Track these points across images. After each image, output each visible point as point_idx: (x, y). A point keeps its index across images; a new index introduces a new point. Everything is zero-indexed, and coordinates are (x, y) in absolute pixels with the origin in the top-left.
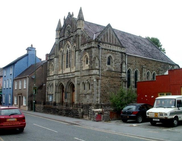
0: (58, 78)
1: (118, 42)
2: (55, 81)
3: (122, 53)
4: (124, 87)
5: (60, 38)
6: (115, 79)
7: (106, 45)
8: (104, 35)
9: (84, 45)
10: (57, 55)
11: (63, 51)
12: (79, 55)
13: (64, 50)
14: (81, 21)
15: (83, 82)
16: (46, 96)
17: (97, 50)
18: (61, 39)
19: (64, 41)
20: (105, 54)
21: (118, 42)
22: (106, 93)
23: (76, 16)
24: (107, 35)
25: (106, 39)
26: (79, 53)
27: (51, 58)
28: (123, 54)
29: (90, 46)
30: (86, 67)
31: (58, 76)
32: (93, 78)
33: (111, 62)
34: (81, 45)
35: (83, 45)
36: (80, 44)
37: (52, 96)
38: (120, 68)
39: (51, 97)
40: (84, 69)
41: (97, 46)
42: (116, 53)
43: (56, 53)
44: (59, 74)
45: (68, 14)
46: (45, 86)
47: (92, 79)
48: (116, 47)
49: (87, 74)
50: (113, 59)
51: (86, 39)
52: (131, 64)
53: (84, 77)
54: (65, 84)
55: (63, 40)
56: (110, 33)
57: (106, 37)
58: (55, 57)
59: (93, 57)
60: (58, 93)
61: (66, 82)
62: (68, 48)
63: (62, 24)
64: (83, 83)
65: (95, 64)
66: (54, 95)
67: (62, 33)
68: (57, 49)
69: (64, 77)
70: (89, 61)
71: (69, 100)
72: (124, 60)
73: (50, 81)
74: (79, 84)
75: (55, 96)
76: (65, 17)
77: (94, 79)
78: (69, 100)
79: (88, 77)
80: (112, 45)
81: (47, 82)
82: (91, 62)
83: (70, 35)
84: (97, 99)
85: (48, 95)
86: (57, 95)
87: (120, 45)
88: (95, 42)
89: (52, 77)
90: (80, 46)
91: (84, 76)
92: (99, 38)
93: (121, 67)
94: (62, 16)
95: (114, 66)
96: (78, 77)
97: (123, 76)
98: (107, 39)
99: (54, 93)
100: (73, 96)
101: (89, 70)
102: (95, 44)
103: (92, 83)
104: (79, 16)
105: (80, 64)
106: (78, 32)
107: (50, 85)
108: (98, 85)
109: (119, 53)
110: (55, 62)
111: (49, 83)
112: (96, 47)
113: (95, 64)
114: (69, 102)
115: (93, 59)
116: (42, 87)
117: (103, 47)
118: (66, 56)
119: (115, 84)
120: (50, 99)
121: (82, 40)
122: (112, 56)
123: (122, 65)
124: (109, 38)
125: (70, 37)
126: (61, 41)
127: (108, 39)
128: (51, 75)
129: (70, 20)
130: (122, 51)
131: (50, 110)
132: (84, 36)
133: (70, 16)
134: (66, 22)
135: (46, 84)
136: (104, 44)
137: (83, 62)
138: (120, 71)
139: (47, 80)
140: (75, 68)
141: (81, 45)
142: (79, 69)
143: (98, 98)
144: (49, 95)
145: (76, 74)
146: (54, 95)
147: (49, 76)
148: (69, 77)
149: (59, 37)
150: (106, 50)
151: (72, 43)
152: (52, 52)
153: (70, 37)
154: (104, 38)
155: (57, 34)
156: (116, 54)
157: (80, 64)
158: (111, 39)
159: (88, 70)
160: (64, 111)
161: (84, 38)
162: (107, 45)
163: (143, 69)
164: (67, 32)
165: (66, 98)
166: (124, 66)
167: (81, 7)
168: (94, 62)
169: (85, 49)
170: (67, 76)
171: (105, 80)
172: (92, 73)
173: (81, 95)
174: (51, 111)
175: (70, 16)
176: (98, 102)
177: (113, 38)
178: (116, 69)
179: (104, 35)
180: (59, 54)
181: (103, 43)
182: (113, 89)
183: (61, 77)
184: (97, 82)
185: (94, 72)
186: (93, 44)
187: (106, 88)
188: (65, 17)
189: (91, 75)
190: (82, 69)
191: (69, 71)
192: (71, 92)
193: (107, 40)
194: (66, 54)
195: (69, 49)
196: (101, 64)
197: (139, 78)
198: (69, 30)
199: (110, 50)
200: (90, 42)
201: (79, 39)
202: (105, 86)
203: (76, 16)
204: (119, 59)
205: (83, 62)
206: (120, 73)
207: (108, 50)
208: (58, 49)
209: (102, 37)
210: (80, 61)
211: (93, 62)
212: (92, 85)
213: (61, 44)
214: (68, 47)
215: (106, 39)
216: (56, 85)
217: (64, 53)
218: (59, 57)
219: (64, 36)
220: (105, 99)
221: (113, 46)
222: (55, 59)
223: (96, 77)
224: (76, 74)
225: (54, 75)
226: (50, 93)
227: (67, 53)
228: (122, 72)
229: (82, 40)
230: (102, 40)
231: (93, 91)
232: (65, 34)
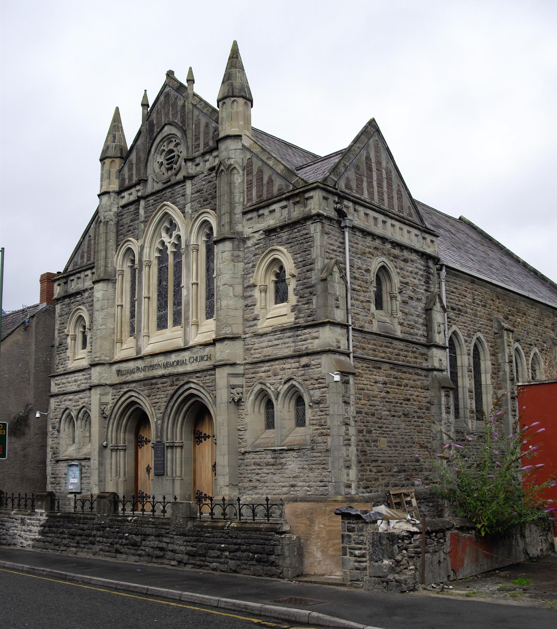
0: (116, 380)
2: (101, 395)
3: (424, 255)
4: (444, 415)
5: (119, 193)
6: (408, 378)
7: (366, 215)
8: (357, 167)
9: (261, 212)
10: (110, 269)
11: (142, 247)
12: (235, 259)
13: (147, 246)
14: (241, 101)
15: (262, 390)
16: (49, 470)
17: (334, 231)
18: (126, 194)
19: (142, 203)
20: (364, 253)
22: (376, 441)
23: (209, 90)
24: (370, 169)
25: (365, 184)
26: (236, 253)
27: (73, 287)
28: (431, 264)
29: (297, 213)
31: (115, 368)
32: (324, 370)
33: (386, 298)
34: (244, 213)
36: (239, 209)
37: (81, 467)
38: (423, 324)
39: (76, 471)
40: (263, 325)
41: (333, 214)
42: (406, 254)
43: (102, 263)
44: (117, 357)
46: (44, 418)
47: (314, 372)
48: (406, 228)
50: (396, 280)
51: (270, 181)
52: (459, 310)
53: (266, 367)
55: (139, 199)
56: (379, 163)
57: (365, 179)
58: (94, 283)
59: (318, 265)
60: (115, 449)
61: (162, 398)
62: (164, 234)
63: (132, 127)
64: (263, 395)
65: (331, 301)
66: (94, 462)
67: (130, 169)
68: (107, 241)
70: (292, 285)
71: (178, 484)
72: (434, 289)
73: (71, 397)
74: (238, 403)
75: (101, 464)
76: (145, 97)
77: (328, 369)
78: (178, 484)
79: (291, 364)
81: (53, 401)
82: (307, 291)
83: (176, 175)
85: (57, 461)
86: (108, 461)
88: (325, 194)
90: (238, 216)
91: (268, 361)
92: (340, 176)
93: (428, 324)
94: (129, 104)
95: (400, 314)
96: (234, 365)
97: (437, 365)
98: (370, 184)
99: (92, 448)
100: (195, 460)
101: (296, 328)
102: (324, 203)
103: (317, 394)
104: (228, 78)
105: (241, 303)
106: (223, 155)
107: (69, 414)
108: (346, 403)
109: (414, 257)
110: (97, 306)
111: (63, 407)
113: (329, 297)
114: (178, 492)
115: (314, 277)
116: (27, 425)
118: (155, 269)
119: (409, 400)
120: (73, 480)
121: (249, 189)
122: (390, 266)
123: (428, 311)
124: (375, 184)
125: (178, 183)
126: (123, 207)
127: (373, 188)
128: (72, 365)
129: (174, 105)
130: (428, 251)
132: (260, 171)
133: (176, 91)
134: (154, 115)
135: (45, 408)
137: (256, 293)
138: (423, 340)
139: (54, 389)
142: (238, 329)
143: (348, 467)
144: (63, 465)
145: (222, 352)
146: (94, 462)
147: (61, 370)
149: (115, 187)
150: (369, 239)
152: (78, 259)
153: (178, 183)
154: (360, 181)
155: (105, 177)
156: (405, 261)
157: (241, 303)
158: (385, 189)
159: (291, 329)
160: (179, 540)
161: (260, 179)
162: (372, 213)
163: (501, 337)
164: (157, 160)
165: (160, 471)
166: (438, 317)
168: (326, 290)
169: (269, 232)
170: (166, 366)
171: (373, 380)
172: (315, 345)
173: (252, 455)
174: (93, 543)
175: (176, 91)
176: (349, 486)
177: (390, 185)
178: (408, 329)
179: (357, 167)
180: (119, 262)
181: (355, 203)
182: (403, 425)
183: (132, 372)
184: (341, 387)
185: (327, 336)
186: (316, 203)
187: (375, 419)
188: (145, 97)
189: (308, 354)
191: (132, 353)
192: (188, 443)
193: (371, 194)
194: (155, 262)
195: (173, 240)
196: (353, 301)
197: (489, 376)
198: (171, 151)
199: (384, 240)
200: (298, 194)
201: (230, 184)
202: (373, 409)
203: (209, 90)
204: (416, 281)
205: (256, 293)
208: (112, 242)
209: (351, 174)
210: (239, 289)
211: (319, 288)
212: (318, 403)
213: (126, 220)
214: (168, 231)
215: (365, 184)
217: (145, 258)
218: (119, 278)
219: (143, 181)
222: (99, 287)
223: (339, 362)
224: (222, 352)
225: (93, 365)
226: (70, 451)
228: (430, 345)
229: (249, 189)
230: (351, 189)
231: (322, 434)
232: (149, 171)
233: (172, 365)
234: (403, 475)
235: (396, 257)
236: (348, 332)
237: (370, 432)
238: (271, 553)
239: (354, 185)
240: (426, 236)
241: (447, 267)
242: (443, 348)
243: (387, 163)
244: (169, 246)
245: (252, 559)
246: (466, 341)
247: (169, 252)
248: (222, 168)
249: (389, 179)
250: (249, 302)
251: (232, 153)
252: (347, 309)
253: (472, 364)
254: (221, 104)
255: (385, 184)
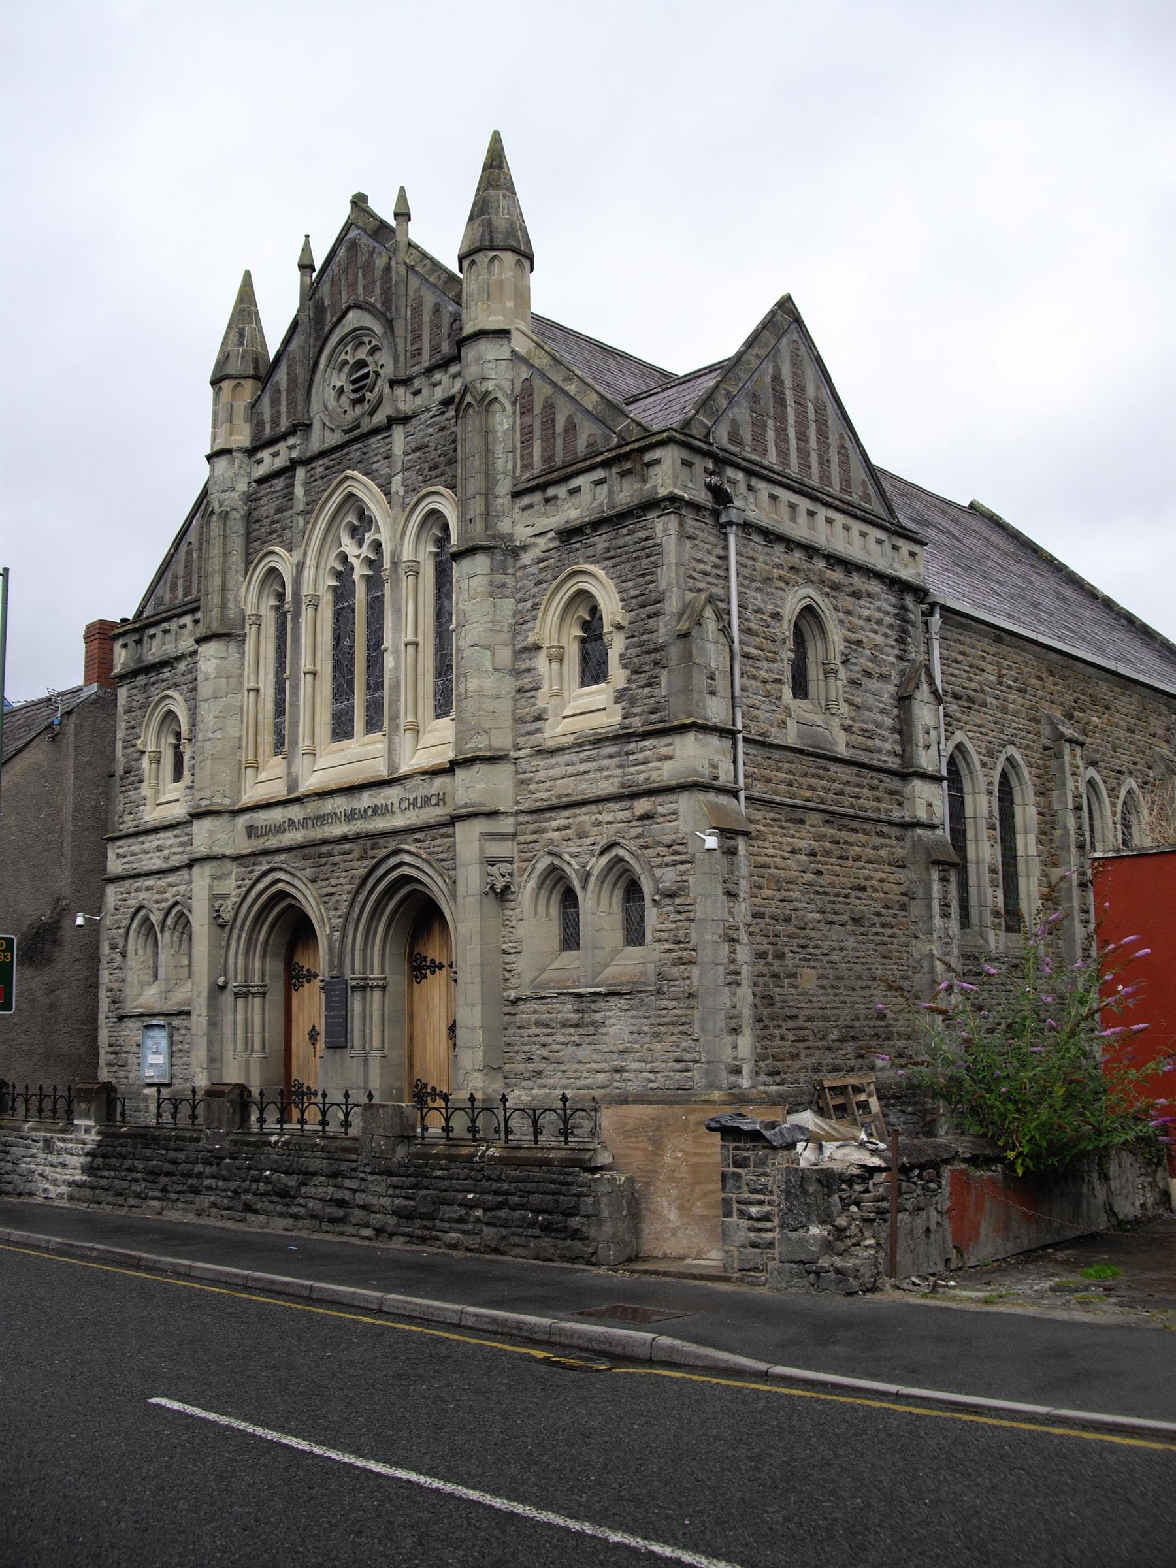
0: (245, 846)
1: (864, 483)
4: (938, 921)
5: (251, 452)
6: (861, 842)
8: (755, 398)
9: (551, 492)
10: (232, 613)
11: (300, 567)
12: (496, 591)
13: (310, 565)
14: (509, 258)
15: (553, 869)
16: (103, 1036)
17: (705, 532)
18: (265, 454)
19: (300, 473)
21: (864, 482)
22: (794, 975)
23: (440, 234)
24: (780, 401)
25: (771, 434)
26: (499, 579)
27: (155, 650)
28: (909, 601)
29: (626, 493)
30: (586, 706)
31: (243, 820)
32: (683, 826)
33: (814, 673)
34: (516, 495)
35: (539, 486)
36: (504, 487)
37: (172, 1031)
38: (893, 729)
39: (160, 1038)
40: (555, 731)
41: (703, 497)
42: (857, 580)
43: (215, 599)
45: (343, 212)
46: (93, 928)
47: (663, 830)
49: (608, 787)
50: (837, 636)
51: (571, 427)
52: (970, 699)
53: (561, 819)
54: (325, 898)
55: (288, 471)
56: (800, 389)
57: (770, 422)
59: (672, 604)
60: (244, 993)
61: (342, 884)
62: (346, 539)
63: (278, 313)
64: (555, 878)
65: (700, 681)
67: (275, 402)
68: (225, 554)
69: (318, 833)
70: (616, 646)
71: (375, 1065)
72: (916, 654)
73: (150, 882)
74: (502, 895)
75: (214, 1023)
76: (307, 249)
77: (693, 824)
78: (375, 1065)
79: (615, 813)
80: (827, 505)
81: (111, 891)
82: (648, 659)
83: (372, 413)
84: (728, 1039)
85: (121, 1018)
86: (228, 1018)
87: (881, 512)
88: (685, 454)
89: (168, 839)
90: (503, 501)
91: (567, 806)
92: (718, 417)
93: (904, 729)
94: (272, 261)
95: (844, 708)
96: (493, 814)
97: (922, 815)
99: (193, 991)
100: (411, 1016)
101: (624, 736)
102: (684, 473)
103: (669, 877)
104: (481, 209)
105: (509, 684)
106: (472, 371)
107: (147, 919)
108: (731, 895)
109: (874, 586)
110: (205, 690)
112: (696, 507)
113: (695, 673)
115: (664, 629)
116: (57, 942)
117: (754, 515)
119: (863, 889)
120: (154, 1059)
121: (527, 443)
122: (824, 605)
123: (904, 700)
124: (792, 433)
125: (376, 431)
126: (261, 481)
127: (787, 441)
128: (151, 815)
129: (368, 266)
130: (905, 574)
131: (188, 1175)
132: (550, 407)
133: (370, 239)
134: (325, 289)
135: (95, 905)
136: (763, 488)
137: (541, 663)
138: (893, 763)
139: (115, 866)
140: (484, 703)
141: (516, 495)
142: (502, 740)
143: (735, 1031)
145: (469, 787)
146: (199, 1020)
147: (128, 825)
148: (381, 824)
149: (242, 438)
151: (397, 481)
152: (164, 591)
153: (376, 431)
154: (759, 427)
155: (222, 417)
156: (856, 595)
158: (813, 443)
159: (614, 738)
161: (549, 423)
162: (785, 495)
163: (1059, 756)
164: (331, 383)
166: (925, 714)
167: (496, 138)
168: (687, 657)
169: (569, 534)
170: (350, 816)
172: (666, 773)
173: (533, 1005)
174: (196, 1191)
175: (370, 239)
176: (737, 1071)
177: (823, 436)
179: (755, 398)
181: (749, 473)
182: (851, 942)
183: (279, 830)
184: (721, 863)
185: (690, 754)
186: (667, 474)
187: (791, 929)
188: (307, 249)
189: (650, 793)
190: (533, 740)
192: (398, 980)
193: (783, 454)
194: (327, 598)
195: (365, 551)
196: (746, 681)
197: (1032, 838)
198: (362, 364)
199: (810, 550)
200: (630, 455)
201: (486, 433)
203: (440, 234)
204: (879, 639)
205: (541, 663)
206: (896, 784)
207: (790, 543)
208: (236, 556)
209: (742, 413)
210: (505, 655)
211: (674, 652)
212: (672, 895)
213: (267, 509)
215: (771, 434)
216: (216, 915)
217: (306, 589)
218: (251, 632)
219: (301, 427)
220: (790, 1036)
221: (832, 514)
222: (210, 649)
223: (715, 809)
224: (469, 787)
225: (197, 815)
226: (149, 997)
227: (342, 592)
229: (527, 443)
230: (741, 444)
231: (679, 962)
233: (363, 815)
234: (850, 1047)
235: (835, 587)
236: (735, 746)
237: (780, 956)
238: (572, 1212)
239: (747, 434)
240: (900, 542)
241: (944, 608)
242: (936, 779)
243: (818, 388)
244: (356, 563)
245: (533, 1224)
246: (984, 765)
247: (356, 577)
248: (468, 399)
249: (822, 423)
250: (525, 682)
251: (490, 367)
252: (733, 697)
253: (996, 813)
254: (466, 264)
255: (812, 433)
